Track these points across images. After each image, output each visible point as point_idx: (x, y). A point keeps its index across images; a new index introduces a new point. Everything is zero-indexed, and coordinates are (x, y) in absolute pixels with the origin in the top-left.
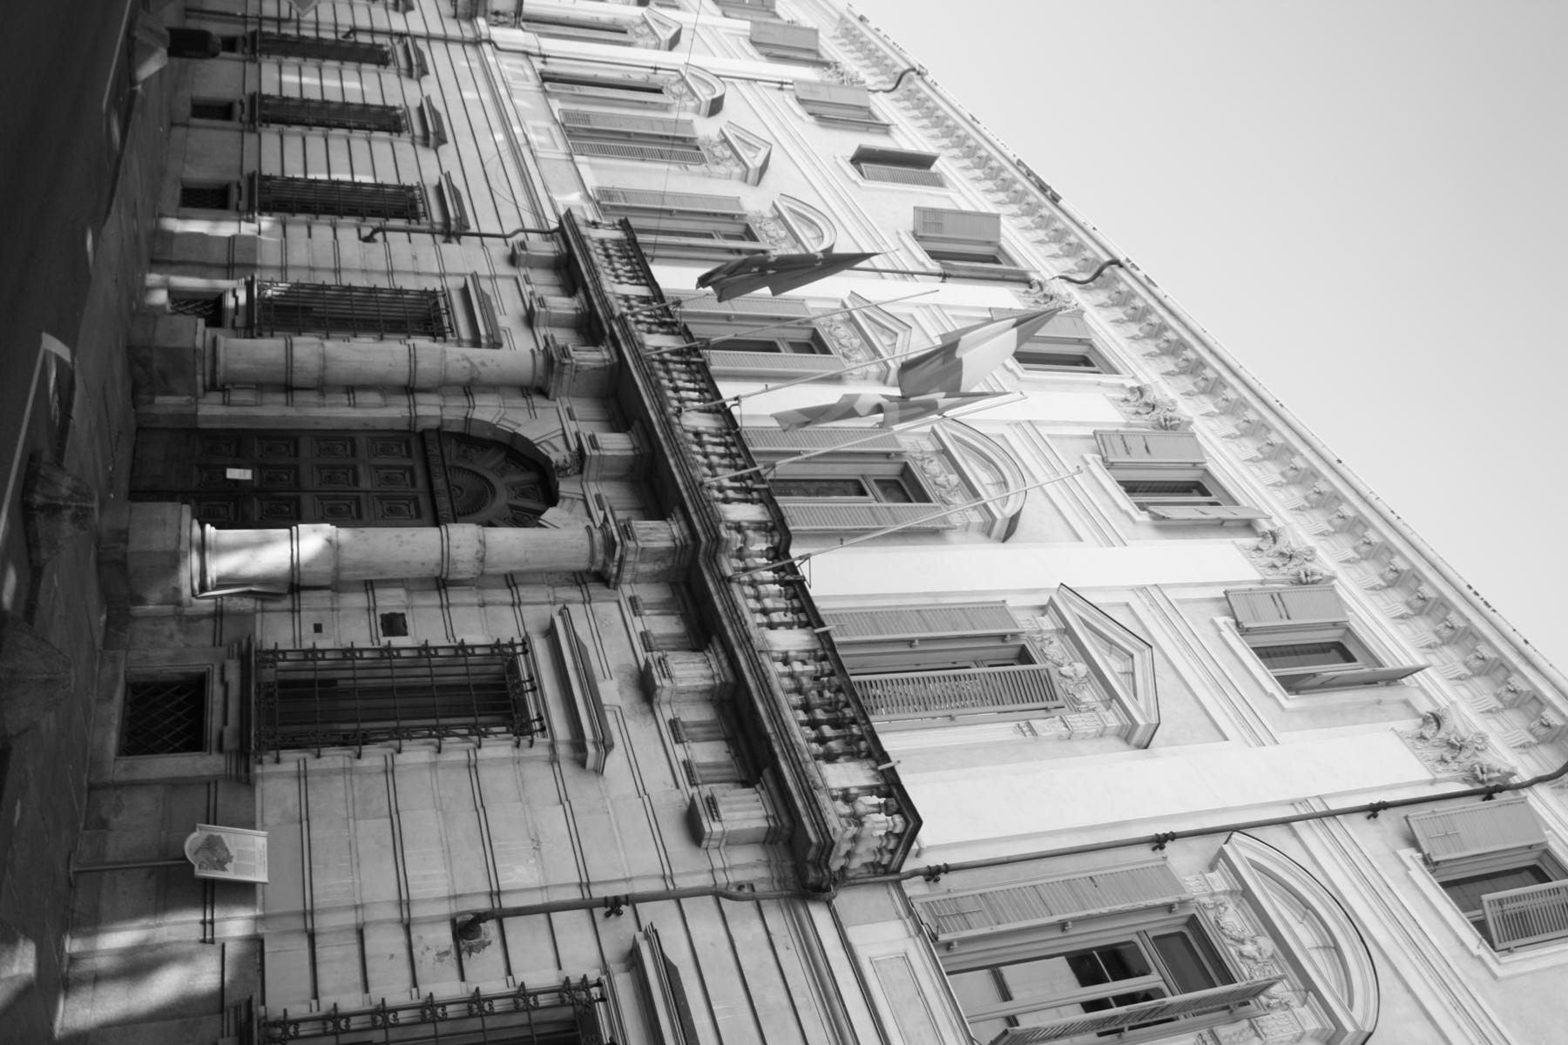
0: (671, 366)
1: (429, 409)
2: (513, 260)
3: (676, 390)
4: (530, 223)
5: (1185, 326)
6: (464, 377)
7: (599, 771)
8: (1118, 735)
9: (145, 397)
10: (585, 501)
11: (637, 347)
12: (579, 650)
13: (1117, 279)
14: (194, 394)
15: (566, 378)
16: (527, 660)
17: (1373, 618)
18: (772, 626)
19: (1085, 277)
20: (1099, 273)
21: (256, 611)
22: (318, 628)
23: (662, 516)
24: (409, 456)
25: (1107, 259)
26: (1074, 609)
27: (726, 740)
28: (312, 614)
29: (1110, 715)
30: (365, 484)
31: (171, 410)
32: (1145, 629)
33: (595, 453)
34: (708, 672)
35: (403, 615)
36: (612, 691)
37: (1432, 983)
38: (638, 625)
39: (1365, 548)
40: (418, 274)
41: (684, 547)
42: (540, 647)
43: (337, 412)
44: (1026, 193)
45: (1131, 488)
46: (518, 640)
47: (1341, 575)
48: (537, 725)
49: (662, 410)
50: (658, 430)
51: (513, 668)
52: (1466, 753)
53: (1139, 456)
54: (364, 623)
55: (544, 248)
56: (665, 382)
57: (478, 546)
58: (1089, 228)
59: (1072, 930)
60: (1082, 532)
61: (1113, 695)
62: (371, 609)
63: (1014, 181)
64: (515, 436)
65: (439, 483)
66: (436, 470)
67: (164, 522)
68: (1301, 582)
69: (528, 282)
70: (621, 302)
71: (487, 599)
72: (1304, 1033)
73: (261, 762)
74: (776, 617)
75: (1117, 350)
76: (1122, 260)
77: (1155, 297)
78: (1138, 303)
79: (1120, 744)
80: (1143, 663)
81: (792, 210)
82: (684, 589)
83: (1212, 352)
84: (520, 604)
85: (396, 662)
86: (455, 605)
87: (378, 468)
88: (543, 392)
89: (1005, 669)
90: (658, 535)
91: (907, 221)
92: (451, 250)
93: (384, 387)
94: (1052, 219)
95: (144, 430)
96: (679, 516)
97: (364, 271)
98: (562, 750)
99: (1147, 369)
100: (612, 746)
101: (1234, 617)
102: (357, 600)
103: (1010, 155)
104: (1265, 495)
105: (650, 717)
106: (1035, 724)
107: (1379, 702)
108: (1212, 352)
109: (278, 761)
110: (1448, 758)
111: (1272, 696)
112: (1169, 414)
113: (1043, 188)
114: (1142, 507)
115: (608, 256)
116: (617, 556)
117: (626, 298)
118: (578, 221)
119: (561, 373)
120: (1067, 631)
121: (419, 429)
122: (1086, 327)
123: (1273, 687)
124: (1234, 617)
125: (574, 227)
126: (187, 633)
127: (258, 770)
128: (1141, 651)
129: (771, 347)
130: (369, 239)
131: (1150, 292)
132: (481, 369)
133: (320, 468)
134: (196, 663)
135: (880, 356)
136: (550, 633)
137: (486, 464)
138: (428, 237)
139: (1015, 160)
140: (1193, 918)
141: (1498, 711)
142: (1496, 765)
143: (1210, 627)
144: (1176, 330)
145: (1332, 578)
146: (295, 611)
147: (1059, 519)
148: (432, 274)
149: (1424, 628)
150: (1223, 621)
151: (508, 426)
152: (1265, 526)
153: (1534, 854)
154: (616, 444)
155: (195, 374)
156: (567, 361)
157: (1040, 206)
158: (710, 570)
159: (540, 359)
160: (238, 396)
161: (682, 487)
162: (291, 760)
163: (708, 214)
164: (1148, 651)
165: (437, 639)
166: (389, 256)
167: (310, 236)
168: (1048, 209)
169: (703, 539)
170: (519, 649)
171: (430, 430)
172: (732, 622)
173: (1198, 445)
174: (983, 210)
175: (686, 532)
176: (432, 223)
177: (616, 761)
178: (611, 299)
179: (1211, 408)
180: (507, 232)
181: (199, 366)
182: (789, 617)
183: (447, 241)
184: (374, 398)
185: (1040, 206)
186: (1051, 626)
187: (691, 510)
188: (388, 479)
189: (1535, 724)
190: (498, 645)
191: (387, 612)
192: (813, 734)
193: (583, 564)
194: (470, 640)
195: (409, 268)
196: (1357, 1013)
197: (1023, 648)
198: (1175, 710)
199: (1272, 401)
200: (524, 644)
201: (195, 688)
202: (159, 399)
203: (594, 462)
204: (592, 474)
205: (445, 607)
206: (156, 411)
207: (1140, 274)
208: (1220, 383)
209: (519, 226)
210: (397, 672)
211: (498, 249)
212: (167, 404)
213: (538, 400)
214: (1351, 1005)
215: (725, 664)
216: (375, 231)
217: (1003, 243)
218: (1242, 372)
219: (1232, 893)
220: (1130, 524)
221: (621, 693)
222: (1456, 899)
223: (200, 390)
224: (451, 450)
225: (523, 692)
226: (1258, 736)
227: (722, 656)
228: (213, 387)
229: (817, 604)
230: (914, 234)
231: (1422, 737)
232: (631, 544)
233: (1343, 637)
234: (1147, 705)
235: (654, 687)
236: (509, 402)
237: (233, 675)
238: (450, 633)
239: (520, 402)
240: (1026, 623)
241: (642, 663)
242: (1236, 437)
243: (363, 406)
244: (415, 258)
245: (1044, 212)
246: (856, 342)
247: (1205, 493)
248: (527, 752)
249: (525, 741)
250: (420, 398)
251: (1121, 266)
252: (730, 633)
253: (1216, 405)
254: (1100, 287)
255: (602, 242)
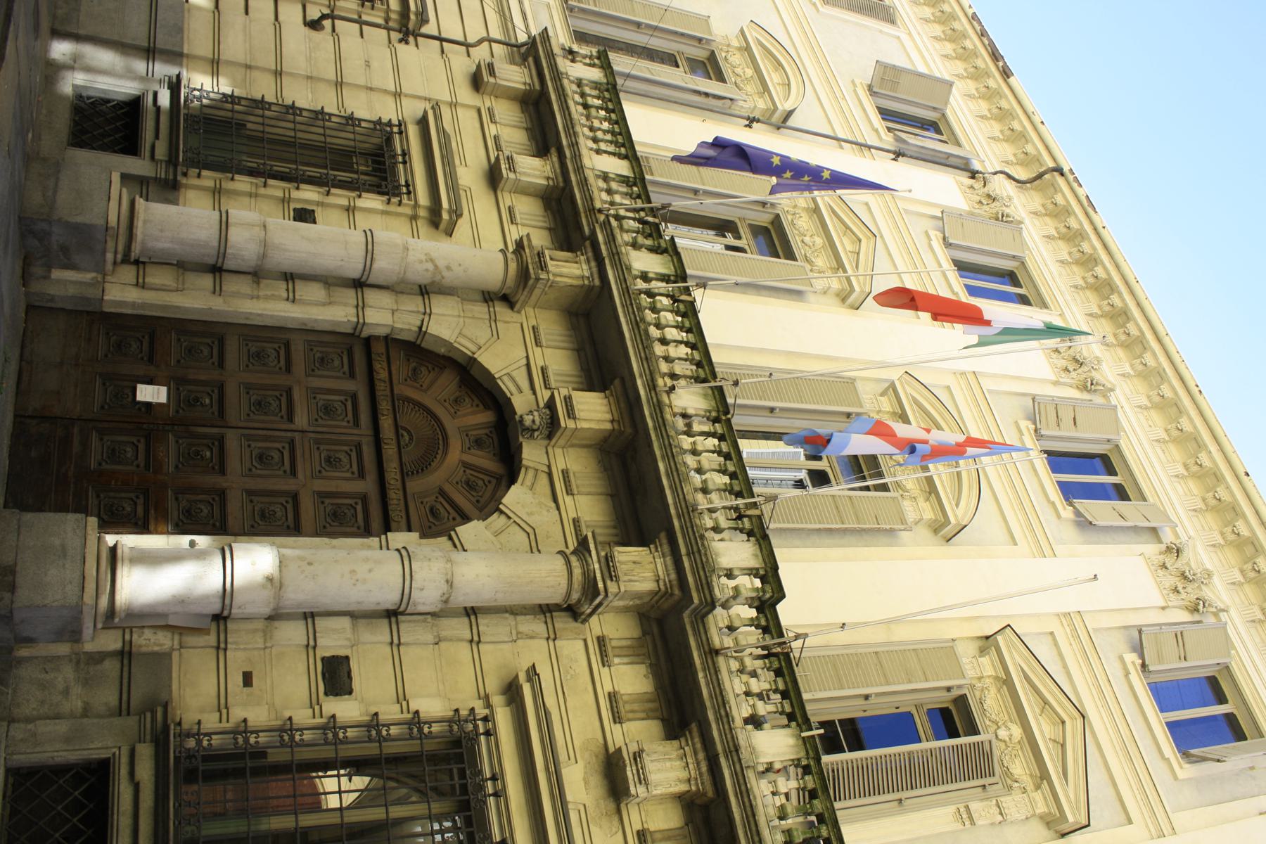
0: (589, 99)
1: (383, 315)
2: (476, 82)
3: (664, 341)
4: (496, 33)
5: (1117, 267)
6: (424, 279)
7: (449, 233)
8: (838, 295)
9: (37, 270)
10: (550, 475)
11: (622, 268)
12: (445, 138)
13: (1056, 189)
14: (100, 268)
15: (537, 292)
16: (488, 743)
17: (1153, 467)
18: (598, 152)
19: (1022, 174)
20: (1040, 176)
21: (173, 649)
22: (248, 679)
23: (643, 541)
24: (352, 375)
25: (1051, 164)
26: (909, 390)
27: (662, 720)
28: (240, 654)
29: (1038, 796)
30: (301, 420)
31: (71, 291)
32: (960, 413)
33: (492, 80)
34: (684, 775)
35: (347, 658)
36: (470, 175)
37: (1138, 797)
38: (514, 233)
39: (1176, 433)
40: (371, 89)
41: (667, 594)
42: (413, 132)
43: (271, 307)
44: (975, 54)
45: (885, 114)
46: (395, 122)
47: (1027, 221)
48: (404, 190)
49: (652, 386)
50: (647, 413)
51: (389, 140)
52: (1085, 368)
53: (1067, 431)
54: (302, 667)
55: (515, 76)
56: (650, 316)
57: (445, 587)
58: (1037, 120)
59: (872, 700)
60: (1134, 814)
61: (1044, 775)
62: (310, 647)
63: (964, 36)
64: (472, 361)
65: (386, 423)
66: (384, 406)
67: (64, 553)
68: (997, 219)
69: (493, 121)
70: (574, 87)
71: (443, 634)
72: (921, 520)
73: (185, 174)
74: (603, 146)
75: (1048, 277)
76: (1066, 170)
77: (1092, 223)
78: (1073, 223)
79: (836, 301)
80: (868, 248)
81: (834, 212)
82: (655, 630)
83: (1138, 304)
84: (479, 642)
85: (299, 119)
86: (407, 644)
87: (317, 391)
88: (507, 300)
89: (855, 464)
90: (640, 570)
91: (866, 73)
92: (406, 52)
93: (331, 281)
94: (998, 93)
95: (37, 310)
96: (666, 548)
97: (309, 78)
98: (422, 213)
99: (1074, 308)
100: (461, 215)
101: (1142, 656)
102: (293, 633)
103: (966, 6)
104: (973, 124)
105: (616, 818)
106: (974, 806)
107: (1252, 768)
108: (1138, 304)
109: (199, 176)
110: (1180, 589)
111: (1168, 760)
112: (1007, 211)
113: (995, 56)
114: (889, 129)
115: (586, 106)
116: (597, 601)
117: (605, 177)
118: (556, 50)
119: (534, 287)
120: (1007, 682)
121: (365, 334)
122: (1023, 244)
123: (1055, 495)
124: (944, 233)
125: (551, 56)
126: (86, 682)
127: (184, 181)
128: (868, 238)
129: (670, 60)
130: (314, 25)
131: (1087, 214)
132: (445, 273)
133: (249, 387)
134: (101, 742)
135: (845, 271)
136: (512, 692)
137: (438, 392)
138: (384, 32)
139: (970, 12)
140: (964, 697)
141: (1165, 442)
142: (1102, 381)
143: (1118, 665)
144: (1091, 245)
145: (1021, 222)
146: (221, 648)
147: (995, 507)
148: (386, 92)
149: (1093, 303)
150: (1132, 658)
151: (467, 347)
152: (1168, 537)
153: (1108, 447)
154: (593, 411)
155: (104, 252)
156: (543, 276)
157: (988, 74)
158: (696, 633)
159: (513, 266)
160: (157, 277)
161: (673, 511)
162: (209, 178)
163: (676, 33)
164: (1080, 720)
165: (331, 108)
166: (338, 58)
167: (247, 13)
168: (996, 81)
169: (696, 601)
170: (396, 129)
171: (377, 338)
172: (718, 719)
173: (1117, 420)
174: (938, 75)
175: (673, 576)
176: (416, 206)
177: (463, 226)
178: (590, 175)
179: (1128, 369)
180: (471, 40)
181: (110, 245)
182: (611, 148)
183: (404, 40)
184: (313, 292)
185: (988, 74)
186: (989, 671)
187: (683, 550)
188: (328, 410)
189: (1249, 566)
190: (379, 122)
191: (328, 654)
192: (580, 100)
193: (557, 597)
194: (360, 114)
195: (362, 82)
196: (960, 512)
197: (778, 216)
198: (1102, 809)
199: (1191, 385)
200: (400, 125)
201: (95, 778)
202: (57, 274)
203: (567, 433)
204: (562, 442)
205: (396, 644)
206: (52, 290)
207: (1080, 191)
208: (1141, 341)
209: (485, 35)
210: (298, 127)
211: (462, 64)
212: (66, 282)
213: (501, 309)
214: (957, 505)
215: (704, 768)
216: (324, 17)
217: (949, 112)
218: (1166, 340)
219: (740, 49)
220: (1053, 518)
221: (586, 782)
222: (1050, 463)
223: (109, 267)
224: (401, 368)
225: (396, 163)
226: (1043, 549)
227: (701, 756)
228: (126, 260)
229: (637, 148)
230: (870, 87)
231: (1164, 566)
232: (543, 276)
233: (1219, 671)
234: (1076, 786)
235: (627, 792)
236: (468, 306)
237: (145, 772)
238: (401, 698)
239: (481, 310)
240: (975, 673)
241: (493, 160)
242: (1146, 408)
243: (303, 302)
244: (368, 64)
245: (991, 83)
246: (819, 241)
247: (939, 132)
248: (392, 208)
249: (395, 200)
250: (372, 296)
251: (1062, 174)
252: (715, 734)
253: (1132, 366)
254: (1035, 189)
255: (579, 83)
